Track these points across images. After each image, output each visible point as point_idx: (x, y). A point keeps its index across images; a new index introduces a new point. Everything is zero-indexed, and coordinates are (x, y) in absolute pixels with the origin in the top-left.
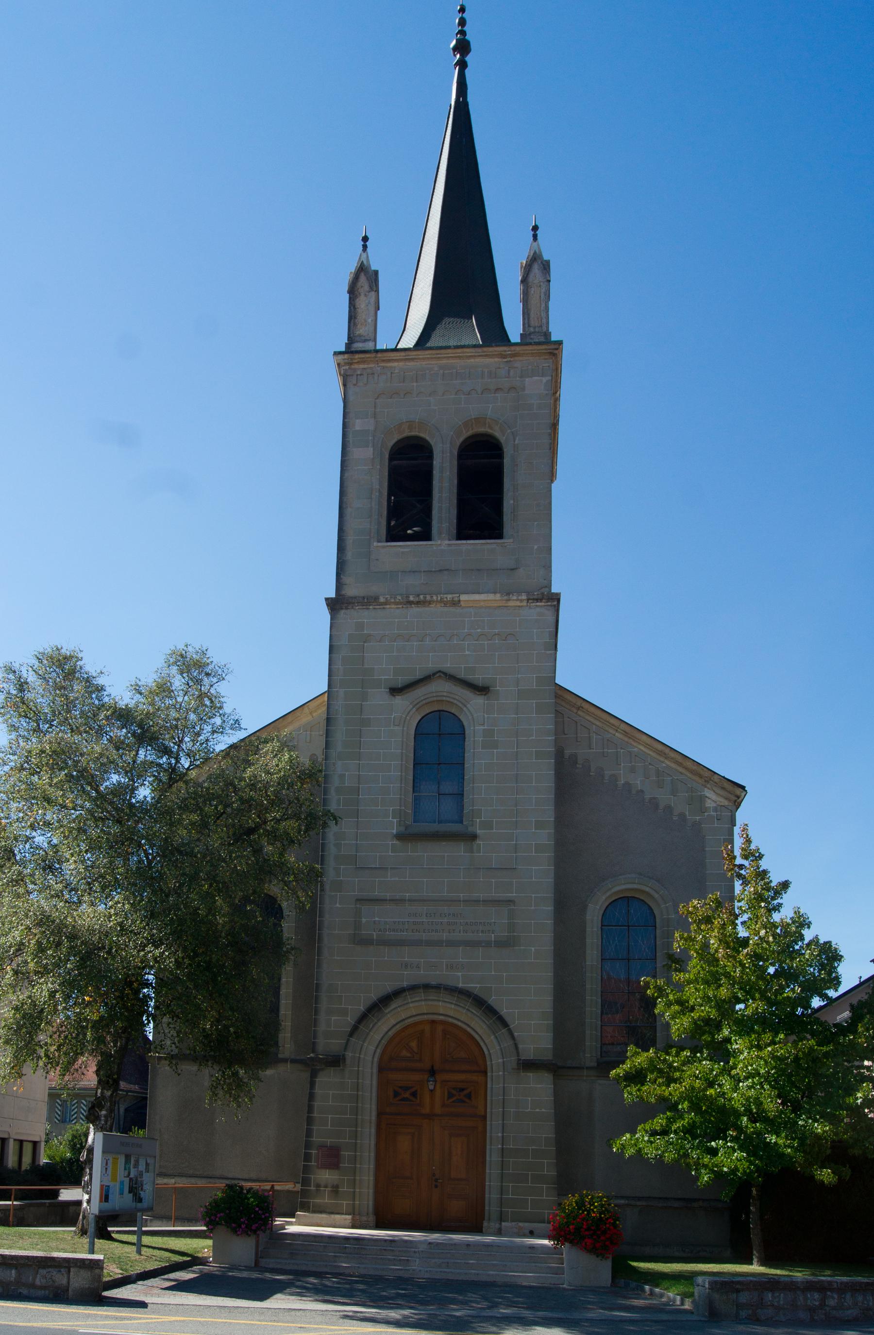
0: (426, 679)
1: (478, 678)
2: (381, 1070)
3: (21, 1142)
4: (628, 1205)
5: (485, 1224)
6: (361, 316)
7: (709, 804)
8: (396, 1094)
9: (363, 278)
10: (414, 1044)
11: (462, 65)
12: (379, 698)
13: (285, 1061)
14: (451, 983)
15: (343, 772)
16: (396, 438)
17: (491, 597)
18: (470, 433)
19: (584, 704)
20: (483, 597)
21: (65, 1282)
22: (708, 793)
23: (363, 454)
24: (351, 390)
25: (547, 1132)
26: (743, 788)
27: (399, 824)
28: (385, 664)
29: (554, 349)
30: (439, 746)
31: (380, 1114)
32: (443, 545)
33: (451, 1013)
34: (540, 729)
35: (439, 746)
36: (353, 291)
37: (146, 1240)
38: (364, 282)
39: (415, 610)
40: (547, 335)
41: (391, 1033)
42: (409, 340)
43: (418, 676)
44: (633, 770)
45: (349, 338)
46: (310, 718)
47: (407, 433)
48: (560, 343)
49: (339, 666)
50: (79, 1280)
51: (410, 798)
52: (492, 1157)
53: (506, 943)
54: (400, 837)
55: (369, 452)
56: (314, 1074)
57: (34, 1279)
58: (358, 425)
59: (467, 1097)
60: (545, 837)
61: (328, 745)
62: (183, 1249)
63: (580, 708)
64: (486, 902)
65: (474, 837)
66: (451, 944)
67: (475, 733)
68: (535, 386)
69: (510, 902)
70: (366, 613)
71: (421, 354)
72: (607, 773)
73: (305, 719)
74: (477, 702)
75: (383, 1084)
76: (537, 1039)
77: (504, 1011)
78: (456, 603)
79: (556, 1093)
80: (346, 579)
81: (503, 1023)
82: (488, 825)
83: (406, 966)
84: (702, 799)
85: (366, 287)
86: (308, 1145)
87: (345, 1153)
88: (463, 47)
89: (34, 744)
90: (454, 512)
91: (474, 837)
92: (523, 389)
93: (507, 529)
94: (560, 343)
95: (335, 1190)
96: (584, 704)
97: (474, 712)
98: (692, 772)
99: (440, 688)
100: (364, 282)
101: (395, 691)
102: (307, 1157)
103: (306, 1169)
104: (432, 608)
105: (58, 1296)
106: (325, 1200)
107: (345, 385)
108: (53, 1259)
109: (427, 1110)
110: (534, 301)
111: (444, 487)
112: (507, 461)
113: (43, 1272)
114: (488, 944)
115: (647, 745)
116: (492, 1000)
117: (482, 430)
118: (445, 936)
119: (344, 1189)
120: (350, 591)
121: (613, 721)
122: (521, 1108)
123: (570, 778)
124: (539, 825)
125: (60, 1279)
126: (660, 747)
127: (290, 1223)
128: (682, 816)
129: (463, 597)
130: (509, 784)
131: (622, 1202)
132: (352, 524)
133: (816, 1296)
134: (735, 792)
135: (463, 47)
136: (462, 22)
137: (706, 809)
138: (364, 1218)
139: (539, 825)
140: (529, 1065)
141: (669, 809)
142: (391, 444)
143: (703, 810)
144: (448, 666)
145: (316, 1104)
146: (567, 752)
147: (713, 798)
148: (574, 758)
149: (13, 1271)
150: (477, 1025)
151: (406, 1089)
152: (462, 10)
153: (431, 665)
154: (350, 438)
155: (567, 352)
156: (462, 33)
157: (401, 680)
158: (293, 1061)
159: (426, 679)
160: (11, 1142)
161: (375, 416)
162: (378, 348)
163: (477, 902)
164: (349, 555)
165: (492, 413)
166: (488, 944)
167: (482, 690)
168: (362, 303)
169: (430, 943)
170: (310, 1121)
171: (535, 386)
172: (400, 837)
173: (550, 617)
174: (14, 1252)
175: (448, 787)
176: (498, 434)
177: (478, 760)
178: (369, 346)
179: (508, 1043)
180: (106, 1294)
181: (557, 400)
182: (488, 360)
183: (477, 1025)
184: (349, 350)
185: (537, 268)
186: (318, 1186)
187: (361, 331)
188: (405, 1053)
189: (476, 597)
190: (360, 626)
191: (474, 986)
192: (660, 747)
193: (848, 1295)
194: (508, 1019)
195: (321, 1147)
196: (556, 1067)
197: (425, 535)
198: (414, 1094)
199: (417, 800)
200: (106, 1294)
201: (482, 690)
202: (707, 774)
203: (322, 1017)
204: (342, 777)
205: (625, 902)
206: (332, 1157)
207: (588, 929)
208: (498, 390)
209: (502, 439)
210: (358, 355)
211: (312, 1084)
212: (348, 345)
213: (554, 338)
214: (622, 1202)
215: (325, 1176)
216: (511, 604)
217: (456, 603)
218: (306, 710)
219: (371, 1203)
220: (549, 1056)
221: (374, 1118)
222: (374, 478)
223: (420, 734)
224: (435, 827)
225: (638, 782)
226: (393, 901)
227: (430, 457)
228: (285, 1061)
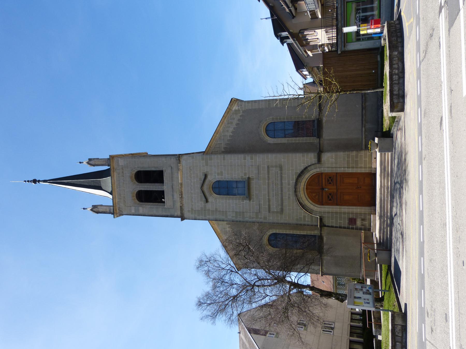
0: (203, 192)
1: (203, 178)
2: (322, 204)
3: (352, 319)
4: (365, 127)
5: (373, 172)
6: (104, 210)
7: (237, 108)
8: (330, 200)
9: (94, 210)
10: (314, 195)
11: (39, 181)
12: (209, 206)
13: (321, 234)
14: (294, 184)
15: (231, 216)
16: (136, 201)
17: (179, 174)
18: (134, 180)
19: (209, 145)
20: (179, 176)
21: (400, 326)
22: (234, 109)
23: (141, 210)
24: (124, 213)
25: (341, 154)
26: (232, 99)
27: (246, 200)
28: (199, 204)
29: (112, 157)
30: (224, 188)
31: (337, 205)
32: (166, 187)
33: (304, 184)
34: (217, 159)
35: (224, 188)
36: (98, 212)
37: (383, 289)
38: (96, 209)
39: (184, 196)
40: (108, 159)
41: (311, 202)
42: (111, 196)
43: (202, 195)
44: (228, 131)
45: (110, 213)
46: (215, 225)
47: (135, 198)
48: (110, 156)
49: (200, 217)
50: (399, 321)
51: (238, 196)
52: (350, 170)
53: (281, 168)
54: (250, 200)
55: (140, 208)
56: (325, 226)
57: (399, 336)
58: (133, 211)
59: (332, 178)
60: (248, 157)
61: (223, 221)
62: (385, 273)
63: (210, 147)
64: (268, 174)
65: (249, 178)
66: (282, 184)
67: (218, 178)
68: (121, 162)
69: (268, 167)
70: (185, 209)
71: (114, 193)
72: (229, 138)
73: (216, 226)
74: (209, 178)
75: (327, 204)
76: (311, 158)
77: (302, 168)
78: (181, 184)
79: (329, 151)
80: (176, 214)
81: (306, 168)
82: (245, 174)
83: (289, 198)
84: (235, 110)
85: (96, 209)
86: (348, 228)
87: (351, 216)
88: (35, 181)
89: (235, 323)
90: (156, 184)
91: (249, 178)
92: (122, 166)
93: (161, 169)
94: (110, 156)
95: (363, 220)
96: (209, 145)
97: (212, 178)
98: (227, 114)
99: (205, 188)
100: (96, 209)
101: (207, 201)
102: (352, 228)
103: (357, 229)
104: (183, 191)
105: (404, 329)
106: (366, 223)
107: (123, 215)
108: (392, 329)
109: (335, 191)
110: (99, 163)
111: (148, 187)
112: (142, 170)
113: (397, 334)
114: (281, 173)
115: (221, 126)
116: (299, 172)
117: (134, 177)
118: (279, 186)
119: (363, 217)
120: (179, 213)
121: (214, 137)
122: (333, 162)
123: (231, 149)
124: (245, 159)
125: (399, 328)
126: (221, 124)
127: (375, 234)
128: (240, 116)
129: (180, 182)
130: (233, 168)
131: (364, 129)
132: (160, 213)
133: (394, 77)
134: (233, 101)
135: (35, 181)
136: (28, 181)
137: (239, 109)
138: (373, 210)
139: (245, 159)
140: (319, 160)
141: (239, 120)
142: (138, 202)
143: (239, 110)
144: (199, 186)
145: (334, 225)
146: (223, 150)
147: (235, 108)
148: (224, 148)
149: (397, 343)
150: (307, 176)
151: (328, 197)
152: (25, 181)
153: (199, 191)
154: (137, 213)
155: (111, 154)
156: (31, 181)
157: (204, 199)
158: (321, 231)
159: (203, 192)
160: (352, 323)
161: (130, 207)
162: (112, 205)
163: (268, 177)
164: (169, 214)
165: (129, 174)
166: (281, 173)
167: (206, 176)
168: (101, 210)
169: (282, 191)
170: (340, 227)
171: (121, 162)
172: (250, 200)
173: (185, 157)
174: (390, 345)
175: (234, 185)
176: (135, 172)
177: (226, 177)
178: (112, 208)
179: (312, 167)
180: (403, 312)
181: (125, 155)
182: (115, 176)
183: (307, 176)
184: (113, 214)
185: (91, 162)
186: (362, 225)
187: (108, 210)
188: (317, 197)
189: (180, 178)
190: (189, 211)
191: (295, 177)
192: (221, 124)
193: (394, 66)
194: (305, 167)
195: (349, 224)
196: (320, 152)
197: (163, 192)
198: (330, 194)
199: (239, 194)
200: (403, 312)
201: (206, 176)
202: (228, 110)
203: (306, 223)
204: (232, 217)
205: (267, 131)
206: (352, 221)
207: (276, 142)
208: (123, 173)
209: (136, 171)
210: (115, 211)
211: (328, 226)
212: (112, 214)
213: (109, 157)
214: (364, 129)
215: (359, 223)
216: (181, 168)
217: (181, 184)
218: (213, 226)
219: (367, 208)
220: (316, 154)
221: (338, 207)
222: (147, 207)
223: (219, 194)
224: (246, 189)
225: (231, 129)
226: (269, 202)
227: (141, 191)
228: (321, 234)
